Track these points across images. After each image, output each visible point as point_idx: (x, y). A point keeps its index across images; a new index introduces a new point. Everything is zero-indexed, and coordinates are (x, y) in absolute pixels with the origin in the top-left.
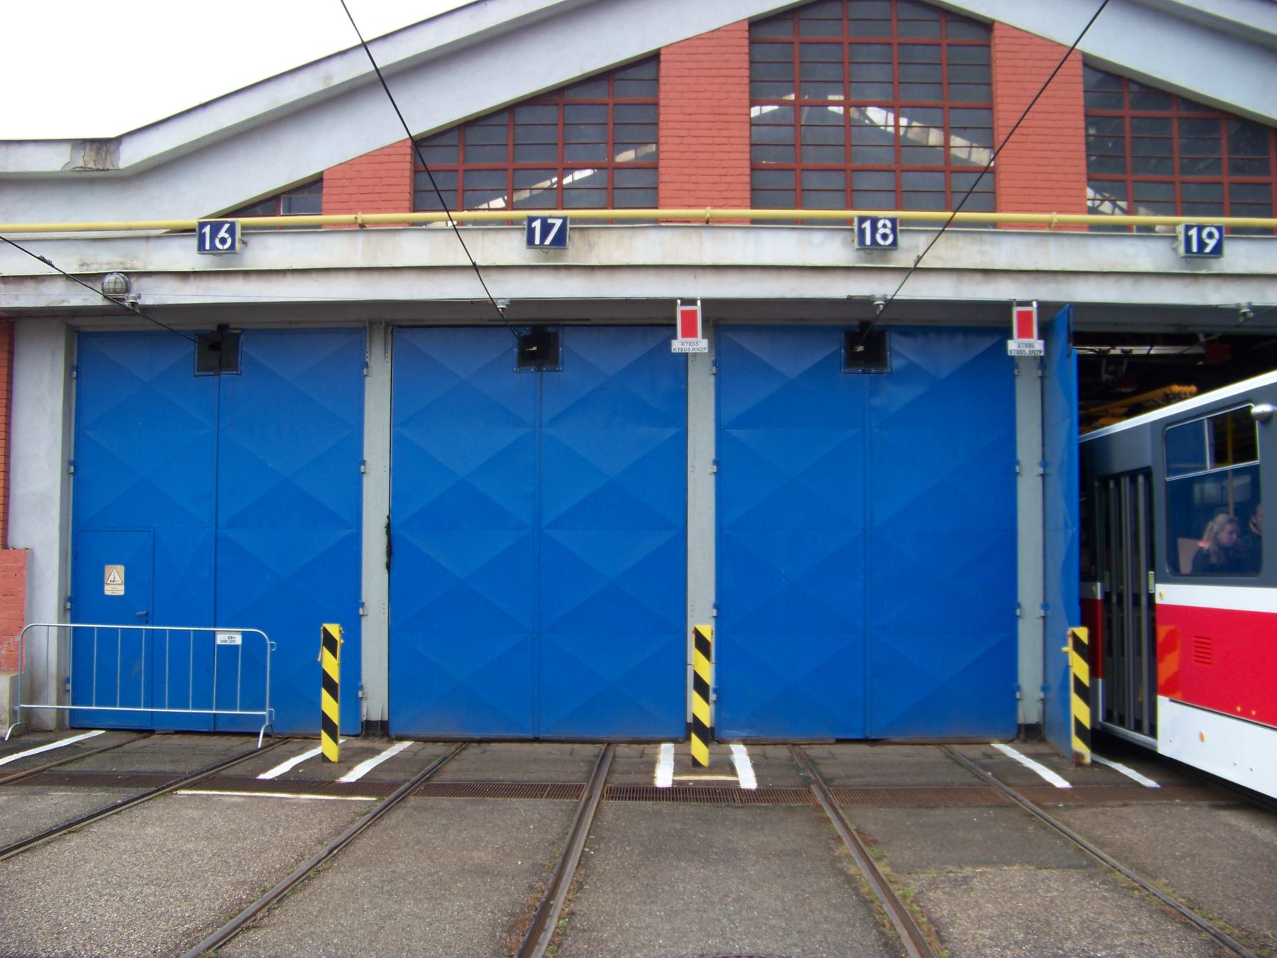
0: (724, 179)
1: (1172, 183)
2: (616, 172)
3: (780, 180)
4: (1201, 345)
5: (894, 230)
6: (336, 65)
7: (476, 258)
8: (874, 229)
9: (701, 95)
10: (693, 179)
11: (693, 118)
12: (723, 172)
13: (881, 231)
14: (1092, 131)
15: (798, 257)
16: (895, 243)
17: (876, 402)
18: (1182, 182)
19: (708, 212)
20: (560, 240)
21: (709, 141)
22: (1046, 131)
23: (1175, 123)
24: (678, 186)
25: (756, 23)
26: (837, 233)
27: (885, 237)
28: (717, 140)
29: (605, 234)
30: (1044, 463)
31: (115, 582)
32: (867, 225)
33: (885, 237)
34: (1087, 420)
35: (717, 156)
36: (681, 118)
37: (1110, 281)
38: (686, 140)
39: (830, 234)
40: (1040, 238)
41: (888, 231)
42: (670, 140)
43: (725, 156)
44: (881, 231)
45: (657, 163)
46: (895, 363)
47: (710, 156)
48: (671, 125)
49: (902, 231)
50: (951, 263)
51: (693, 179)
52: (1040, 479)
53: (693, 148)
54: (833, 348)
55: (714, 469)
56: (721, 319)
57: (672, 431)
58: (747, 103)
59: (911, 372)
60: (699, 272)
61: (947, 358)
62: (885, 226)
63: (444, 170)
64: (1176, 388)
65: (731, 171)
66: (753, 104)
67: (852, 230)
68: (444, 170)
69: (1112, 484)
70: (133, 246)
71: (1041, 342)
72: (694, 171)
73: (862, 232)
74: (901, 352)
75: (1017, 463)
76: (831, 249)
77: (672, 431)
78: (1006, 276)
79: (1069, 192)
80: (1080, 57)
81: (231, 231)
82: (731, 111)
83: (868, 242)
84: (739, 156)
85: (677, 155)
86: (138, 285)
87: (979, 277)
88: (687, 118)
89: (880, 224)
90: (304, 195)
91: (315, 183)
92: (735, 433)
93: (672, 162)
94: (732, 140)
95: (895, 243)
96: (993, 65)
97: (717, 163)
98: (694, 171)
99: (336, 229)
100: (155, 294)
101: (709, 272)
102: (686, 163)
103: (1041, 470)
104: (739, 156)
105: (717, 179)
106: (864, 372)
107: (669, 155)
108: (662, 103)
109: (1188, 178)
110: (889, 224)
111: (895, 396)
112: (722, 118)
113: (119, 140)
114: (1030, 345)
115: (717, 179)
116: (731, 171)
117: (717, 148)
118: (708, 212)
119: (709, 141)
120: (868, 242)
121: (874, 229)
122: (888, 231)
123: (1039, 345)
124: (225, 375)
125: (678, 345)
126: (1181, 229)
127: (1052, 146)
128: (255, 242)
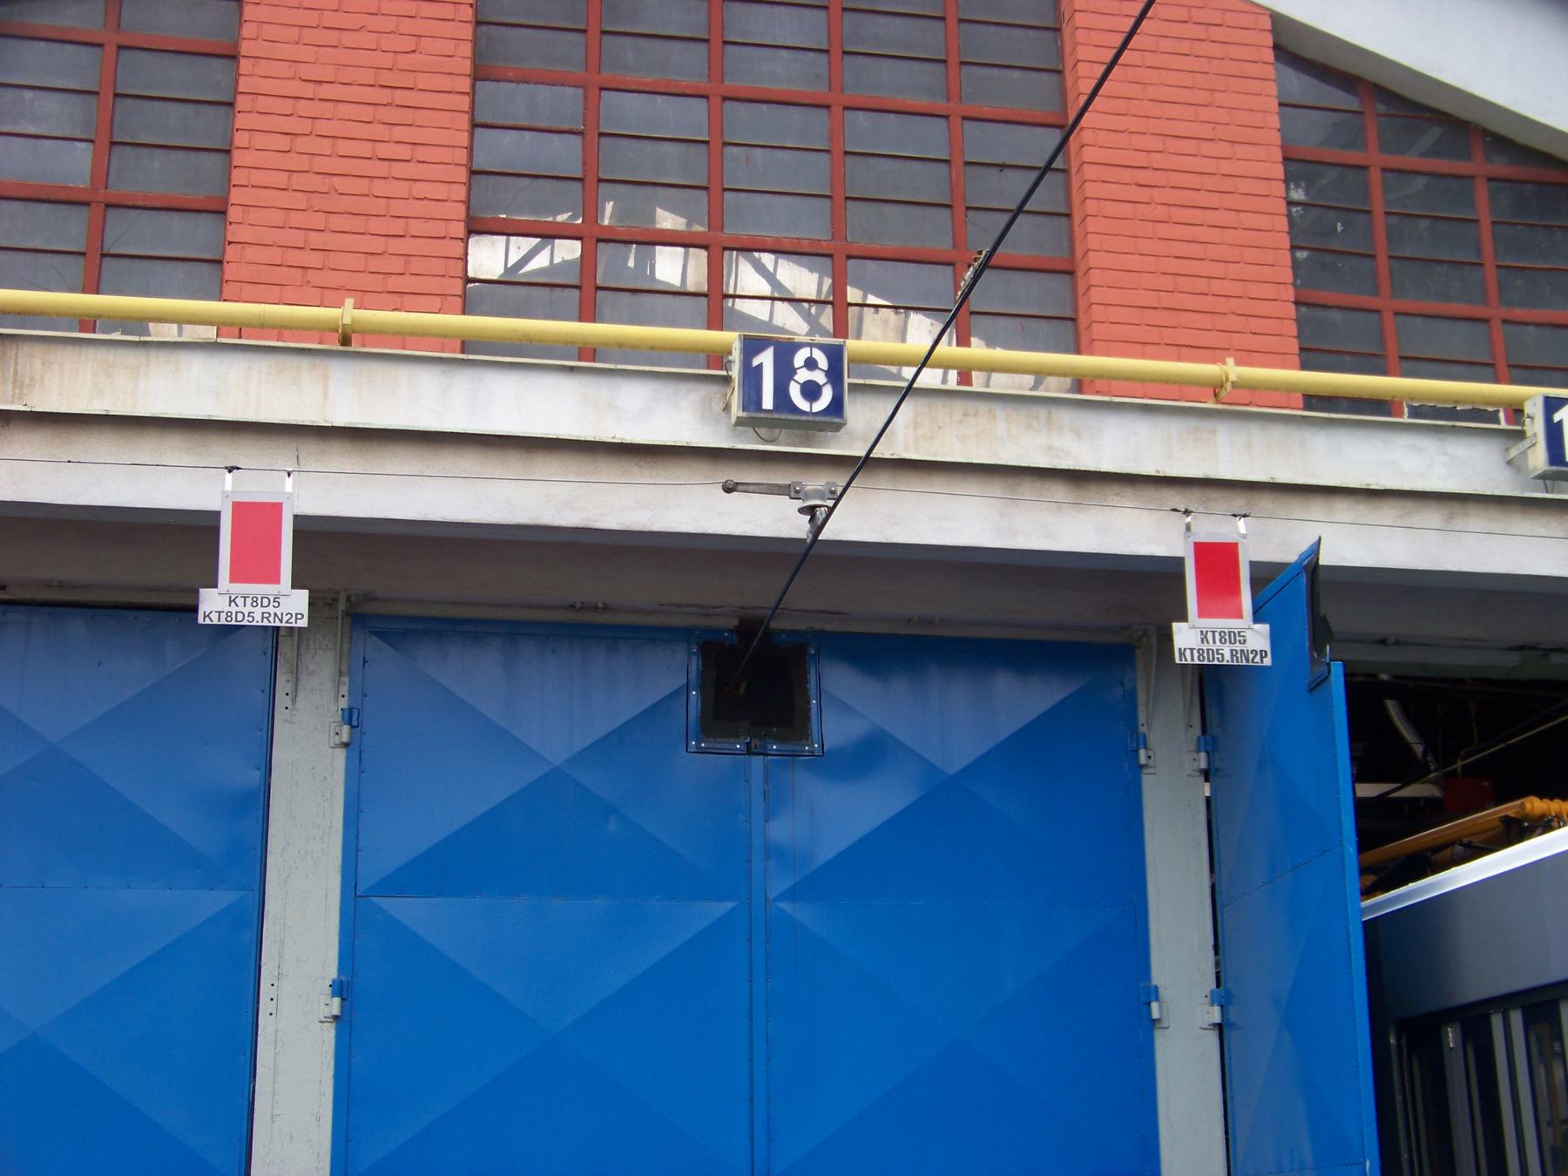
0: (396, 246)
1: (1486, 321)
2: (112, 213)
4: (1434, 782)
5: (834, 374)
8: (784, 372)
9: (349, 39)
10: (316, 240)
11: (326, 91)
12: (397, 227)
13: (803, 375)
14: (1298, 195)
16: (836, 407)
17: (781, 830)
18: (1505, 321)
21: (365, 149)
22: (1195, 181)
23: (1482, 190)
24: (275, 255)
26: (684, 387)
27: (811, 391)
28: (383, 150)
29: (67, 356)
30: (1223, 991)
32: (766, 359)
33: (811, 391)
34: (1395, 840)
35: (379, 187)
36: (295, 88)
37: (1388, 512)
38: (302, 144)
39: (665, 390)
40: (1192, 423)
41: (819, 377)
42: (260, 141)
43: (401, 189)
44: (803, 375)
45: (225, 201)
47: (361, 186)
48: (263, 104)
49: (853, 387)
50: (986, 453)
51: (316, 240)
52: (1213, 1036)
53: (320, 164)
54: (670, 676)
55: (335, 1006)
56: (370, 598)
57: (219, 900)
58: (459, 229)
59: (869, 755)
60: (309, 447)
61: (963, 722)
62: (811, 364)
64: (1535, 805)
65: (416, 227)
66: (477, 227)
67: (727, 380)
69: (1452, 1036)
71: (1264, 628)
72: (319, 220)
73: (752, 377)
74: (845, 705)
75: (1153, 993)
77: (219, 900)
78: (1129, 492)
79: (1255, 324)
80: (1266, 23)
82: (424, 81)
83: (768, 402)
84: (439, 191)
85: (280, 179)
87: (1059, 491)
88: (309, 89)
89: (800, 358)
93: (266, 197)
94: (422, 153)
95: (836, 407)
96: (1067, 30)
97: (379, 206)
98: (319, 220)
101: (336, 448)
102: (300, 200)
103: (1215, 1015)
104: (439, 191)
105: (378, 245)
106: (749, 751)
107: (257, 177)
108: (246, 48)
109: (1519, 313)
110: (823, 362)
111: (833, 815)
112: (400, 97)
114: (1233, 636)
115: (378, 245)
116: (416, 227)
117: (381, 168)
119: (365, 149)
120: (768, 402)
121: (784, 372)
122: (819, 377)
126: (1534, 409)
127: (1210, 216)
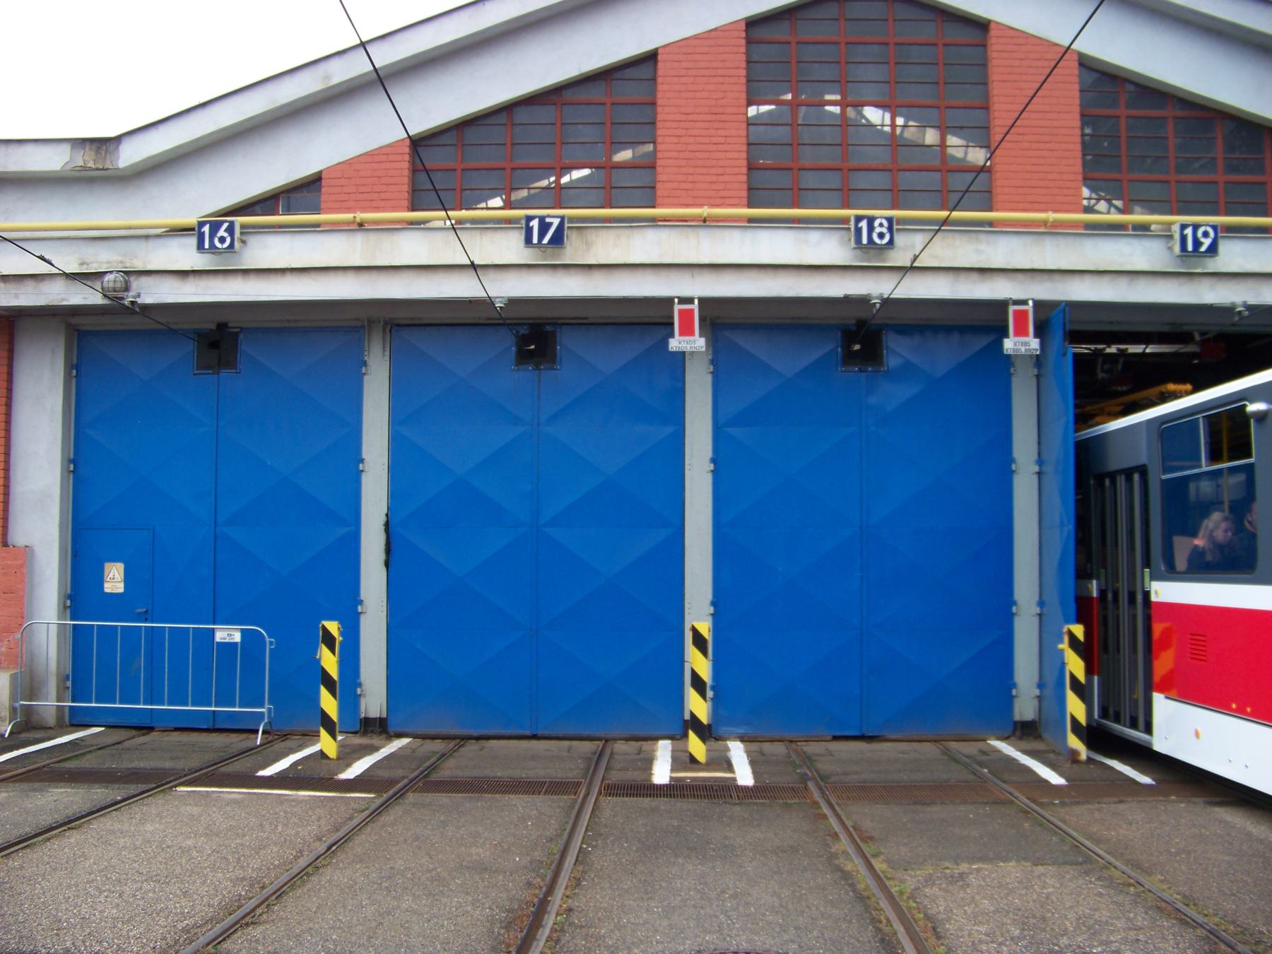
0: (721, 178)
1: (1168, 182)
2: (614, 171)
3: (776, 179)
4: (1196, 343)
5: (890, 229)
6: (335, 65)
7: (474, 257)
8: (871, 228)
9: (698, 95)
10: (690, 178)
11: (690, 117)
12: (720, 171)
13: (878, 230)
14: (1088, 131)
15: (795, 255)
16: (891, 242)
17: (873, 400)
18: (1178, 182)
19: (705, 211)
20: (558, 239)
21: (706, 140)
22: (1042, 131)
23: (1171, 123)
24: (676, 185)
25: (753, 23)
26: (833, 232)
27: (881, 236)
28: (715, 140)
29: (603, 233)
30: (1040, 462)
31: (114, 579)
32: (864, 224)
33: (881, 236)
34: (1083, 419)
35: (714, 155)
36: (678, 117)
37: (1106, 280)
38: (683, 140)
39: (826, 233)
40: (1035, 237)
41: (884, 230)
42: (667, 139)
43: (722, 155)
44: (878, 230)
45: (655, 163)
46: (892, 362)
47: (707, 155)
48: (668, 124)
49: (898, 230)
50: (948, 262)
51: (690, 178)
52: (1036, 477)
53: (691, 148)
54: (830, 346)
55: (712, 467)
56: (718, 317)
57: (669, 429)
58: (744, 102)
59: (907, 370)
60: (696, 271)
61: (943, 356)
62: (881, 225)
63: (442, 169)
64: (1171, 387)
65: (728, 170)
66: (750, 103)
67: (849, 229)
68: (442, 169)
69: (1107, 482)
70: (132, 245)
71: (1037, 340)
72: (691, 170)
73: (858, 231)
74: (897, 351)
75: (1013, 461)
76: (827, 248)
77: (669, 429)
78: (1002, 275)
79: (1065, 191)
80: (1076, 57)
81: (230, 230)
82: (728, 110)
83: (865, 241)
84: (736, 155)
85: (675, 155)
86: (137, 284)
87: (975, 276)
88: (684, 117)
89: (877, 223)
90: (302, 194)
91: (314, 182)
92: (733, 431)
93: (669, 162)
94: (729, 140)
95: (891, 242)
96: (990, 65)
97: (714, 163)
98: (691, 170)
99: (335, 228)
100: (154, 293)
101: (706, 271)
102: (683, 163)
103: (1037, 469)
104: (736, 155)
105: (714, 178)
106: (861, 371)
107: (667, 155)
108: (659, 102)
109: (1184, 177)
110: (885, 223)
111: (892, 395)
112: (719, 117)
113: (118, 139)
114: (1026, 344)
115: (714, 178)
116: (728, 170)
117: (714, 147)
118: (705, 211)
119: (706, 140)
120: (865, 241)
121: (871, 228)
122: (884, 230)
123: (1034, 344)
124: (224, 374)
125: (675, 344)
126: (1176, 228)
127: (1048, 146)
128: (254, 241)
